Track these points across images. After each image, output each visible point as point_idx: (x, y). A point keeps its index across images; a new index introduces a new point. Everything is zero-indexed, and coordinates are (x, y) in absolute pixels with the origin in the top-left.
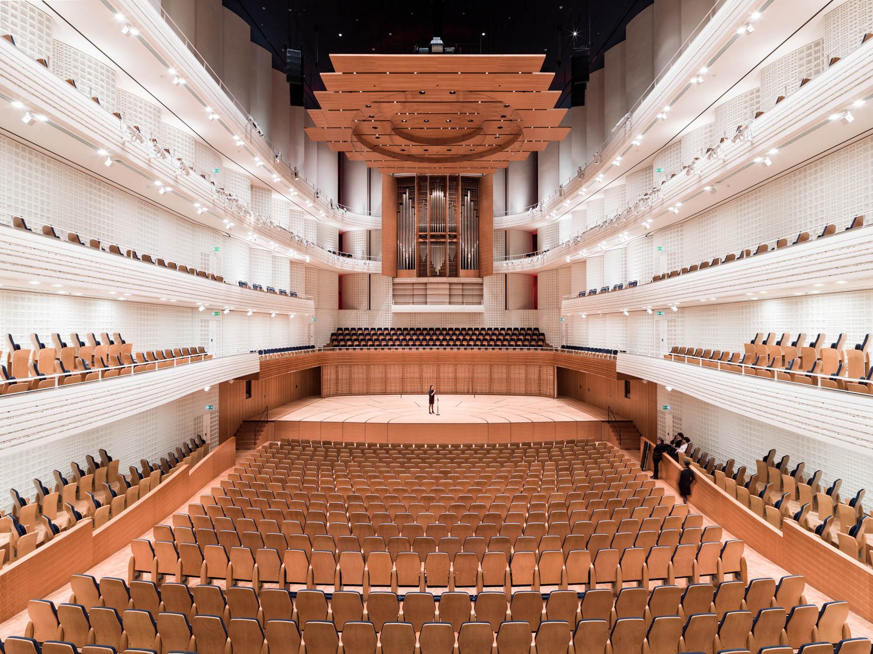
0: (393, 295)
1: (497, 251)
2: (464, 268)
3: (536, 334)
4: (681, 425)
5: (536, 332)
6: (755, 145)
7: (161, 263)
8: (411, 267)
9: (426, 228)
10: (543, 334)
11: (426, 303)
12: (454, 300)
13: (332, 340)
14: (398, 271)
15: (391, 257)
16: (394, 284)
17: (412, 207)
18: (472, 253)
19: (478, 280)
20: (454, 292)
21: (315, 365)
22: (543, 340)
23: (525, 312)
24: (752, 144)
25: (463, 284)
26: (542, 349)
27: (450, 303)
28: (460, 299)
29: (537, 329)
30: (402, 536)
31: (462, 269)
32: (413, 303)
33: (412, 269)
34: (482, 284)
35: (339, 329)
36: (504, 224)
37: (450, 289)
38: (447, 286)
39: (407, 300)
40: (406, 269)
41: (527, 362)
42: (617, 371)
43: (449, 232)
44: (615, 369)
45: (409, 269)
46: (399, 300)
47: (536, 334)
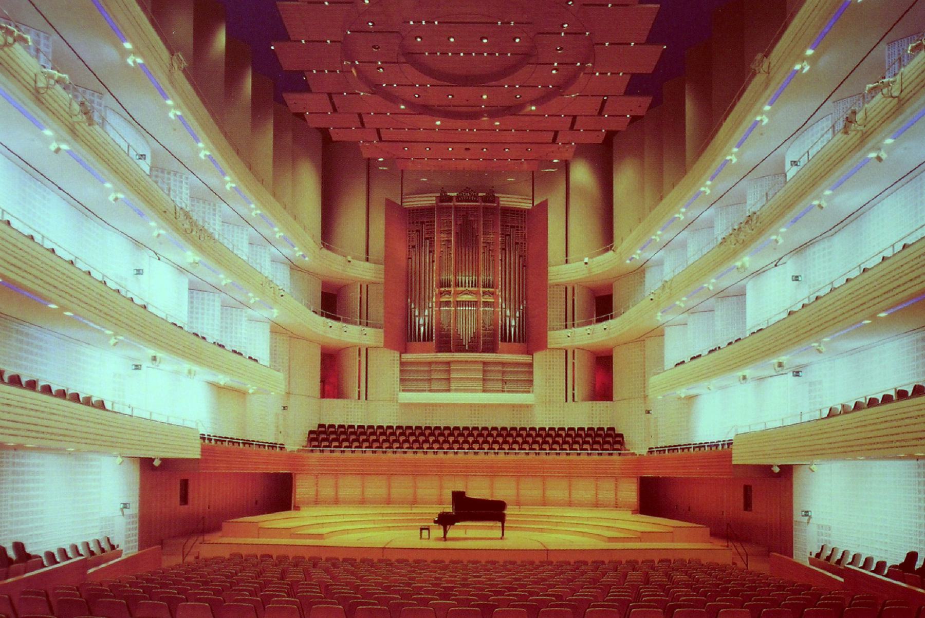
0: (402, 380)
1: (555, 311)
2: (504, 339)
3: (610, 436)
4: (830, 535)
5: (612, 432)
6: (902, 102)
7: (47, 390)
8: (428, 338)
9: (450, 281)
10: (621, 436)
11: (448, 390)
12: (490, 385)
13: (311, 440)
14: (408, 343)
15: (398, 321)
16: (402, 364)
17: (430, 252)
18: (520, 200)
19: (523, 358)
20: (491, 376)
21: (286, 470)
22: (622, 443)
23: (594, 405)
24: (900, 100)
25: (503, 364)
26: (620, 454)
27: (484, 391)
28: (499, 385)
29: (612, 429)
30: (436, 310)
31: (501, 341)
32: (430, 391)
33: (428, 341)
34: (530, 365)
35: (321, 426)
36: (563, 276)
37: (484, 371)
38: (480, 367)
39: (421, 385)
40: (419, 340)
41: (597, 475)
42: (734, 463)
43: (484, 287)
44: (731, 461)
45: (424, 340)
46: (410, 385)
47: (610, 436)
